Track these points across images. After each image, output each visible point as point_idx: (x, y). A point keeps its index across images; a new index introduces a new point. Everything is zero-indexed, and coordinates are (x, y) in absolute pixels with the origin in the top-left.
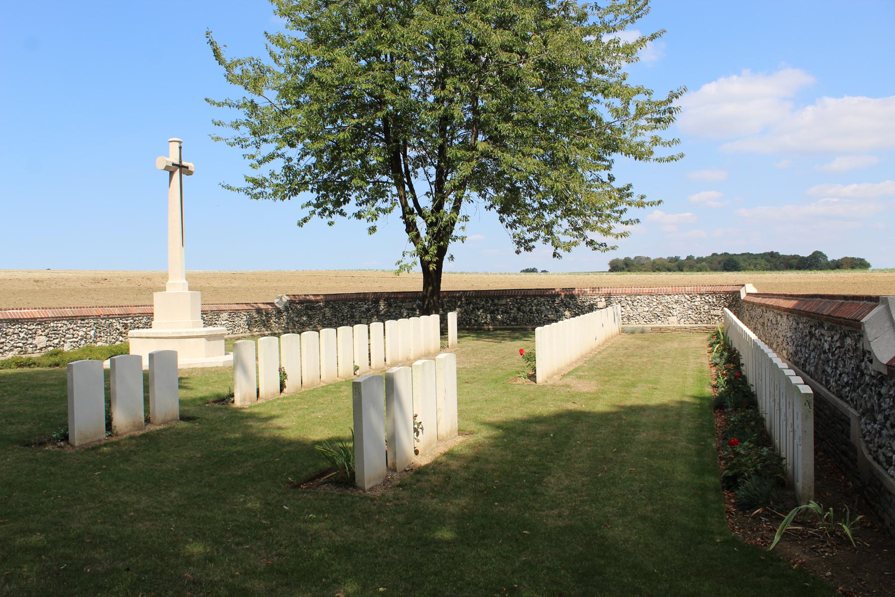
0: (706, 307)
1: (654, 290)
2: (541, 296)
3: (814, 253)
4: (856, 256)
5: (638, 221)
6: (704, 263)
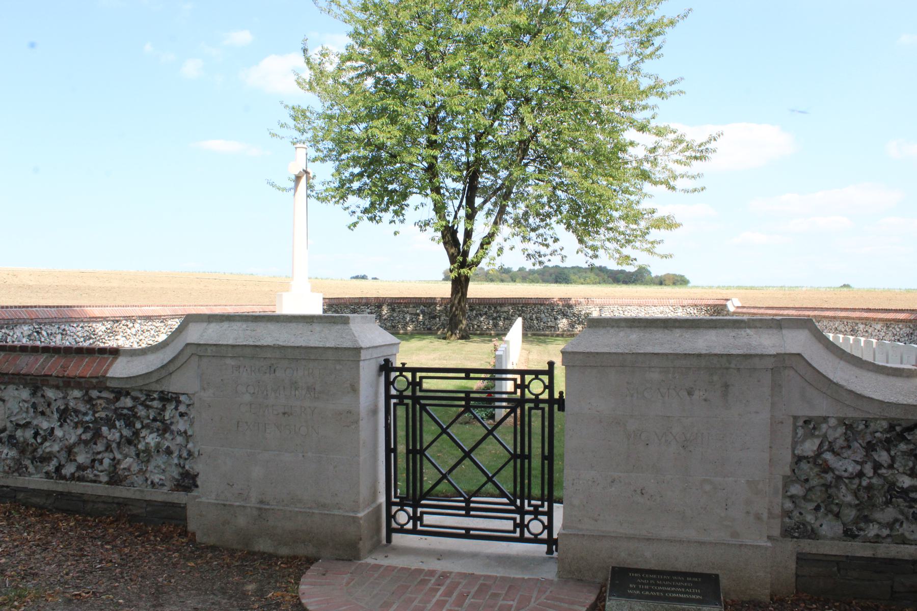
1: (642, 301)
2: (541, 305)
4: (678, 273)
6: (536, 275)
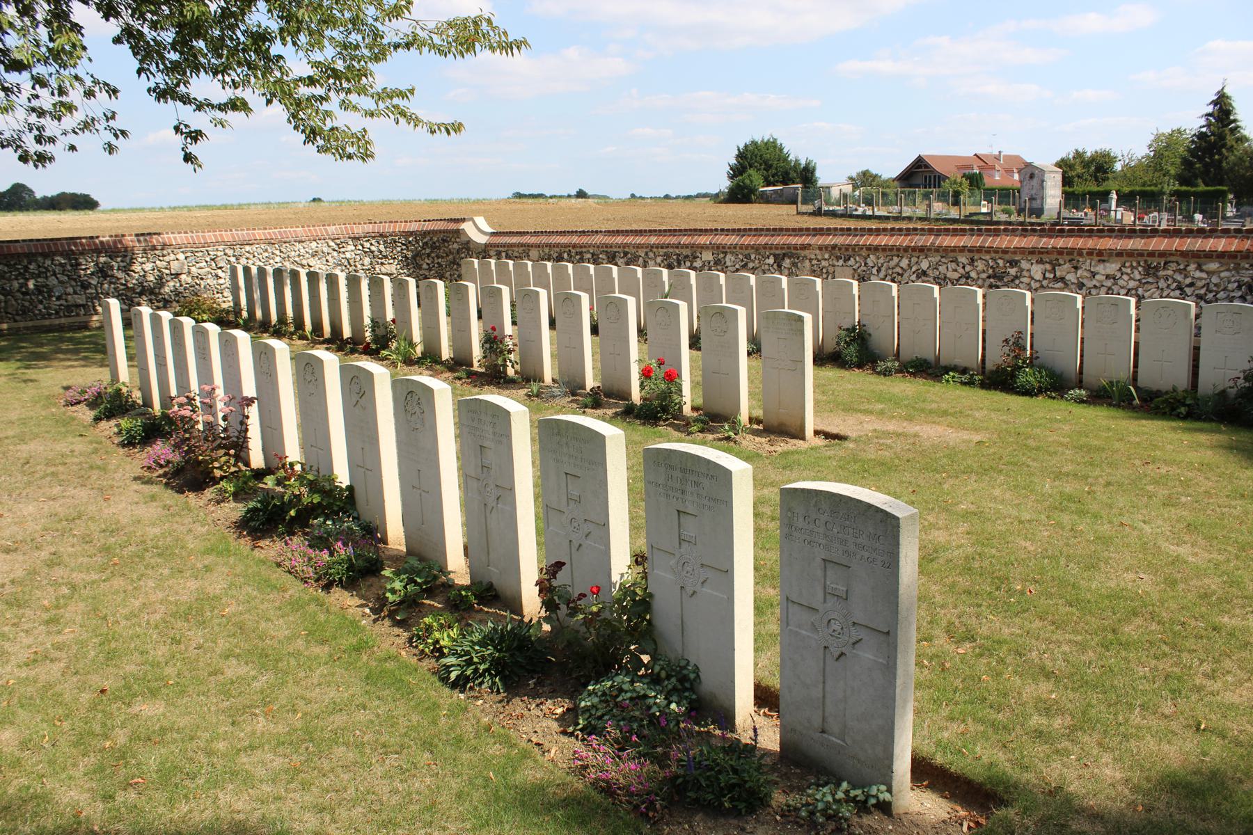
0: (367, 261)
3: (741, 156)
4: (78, 192)
5: (525, 42)
